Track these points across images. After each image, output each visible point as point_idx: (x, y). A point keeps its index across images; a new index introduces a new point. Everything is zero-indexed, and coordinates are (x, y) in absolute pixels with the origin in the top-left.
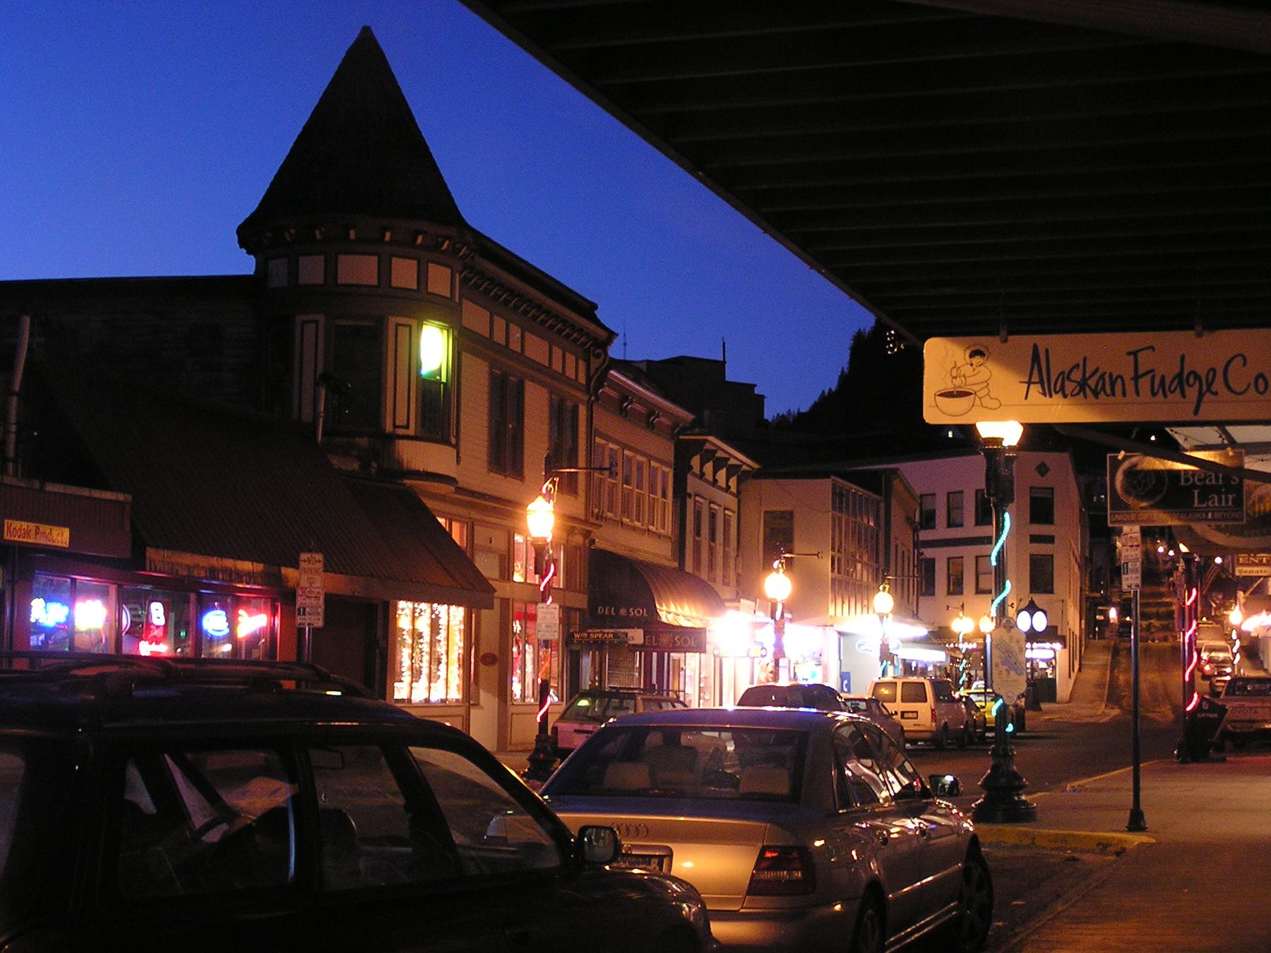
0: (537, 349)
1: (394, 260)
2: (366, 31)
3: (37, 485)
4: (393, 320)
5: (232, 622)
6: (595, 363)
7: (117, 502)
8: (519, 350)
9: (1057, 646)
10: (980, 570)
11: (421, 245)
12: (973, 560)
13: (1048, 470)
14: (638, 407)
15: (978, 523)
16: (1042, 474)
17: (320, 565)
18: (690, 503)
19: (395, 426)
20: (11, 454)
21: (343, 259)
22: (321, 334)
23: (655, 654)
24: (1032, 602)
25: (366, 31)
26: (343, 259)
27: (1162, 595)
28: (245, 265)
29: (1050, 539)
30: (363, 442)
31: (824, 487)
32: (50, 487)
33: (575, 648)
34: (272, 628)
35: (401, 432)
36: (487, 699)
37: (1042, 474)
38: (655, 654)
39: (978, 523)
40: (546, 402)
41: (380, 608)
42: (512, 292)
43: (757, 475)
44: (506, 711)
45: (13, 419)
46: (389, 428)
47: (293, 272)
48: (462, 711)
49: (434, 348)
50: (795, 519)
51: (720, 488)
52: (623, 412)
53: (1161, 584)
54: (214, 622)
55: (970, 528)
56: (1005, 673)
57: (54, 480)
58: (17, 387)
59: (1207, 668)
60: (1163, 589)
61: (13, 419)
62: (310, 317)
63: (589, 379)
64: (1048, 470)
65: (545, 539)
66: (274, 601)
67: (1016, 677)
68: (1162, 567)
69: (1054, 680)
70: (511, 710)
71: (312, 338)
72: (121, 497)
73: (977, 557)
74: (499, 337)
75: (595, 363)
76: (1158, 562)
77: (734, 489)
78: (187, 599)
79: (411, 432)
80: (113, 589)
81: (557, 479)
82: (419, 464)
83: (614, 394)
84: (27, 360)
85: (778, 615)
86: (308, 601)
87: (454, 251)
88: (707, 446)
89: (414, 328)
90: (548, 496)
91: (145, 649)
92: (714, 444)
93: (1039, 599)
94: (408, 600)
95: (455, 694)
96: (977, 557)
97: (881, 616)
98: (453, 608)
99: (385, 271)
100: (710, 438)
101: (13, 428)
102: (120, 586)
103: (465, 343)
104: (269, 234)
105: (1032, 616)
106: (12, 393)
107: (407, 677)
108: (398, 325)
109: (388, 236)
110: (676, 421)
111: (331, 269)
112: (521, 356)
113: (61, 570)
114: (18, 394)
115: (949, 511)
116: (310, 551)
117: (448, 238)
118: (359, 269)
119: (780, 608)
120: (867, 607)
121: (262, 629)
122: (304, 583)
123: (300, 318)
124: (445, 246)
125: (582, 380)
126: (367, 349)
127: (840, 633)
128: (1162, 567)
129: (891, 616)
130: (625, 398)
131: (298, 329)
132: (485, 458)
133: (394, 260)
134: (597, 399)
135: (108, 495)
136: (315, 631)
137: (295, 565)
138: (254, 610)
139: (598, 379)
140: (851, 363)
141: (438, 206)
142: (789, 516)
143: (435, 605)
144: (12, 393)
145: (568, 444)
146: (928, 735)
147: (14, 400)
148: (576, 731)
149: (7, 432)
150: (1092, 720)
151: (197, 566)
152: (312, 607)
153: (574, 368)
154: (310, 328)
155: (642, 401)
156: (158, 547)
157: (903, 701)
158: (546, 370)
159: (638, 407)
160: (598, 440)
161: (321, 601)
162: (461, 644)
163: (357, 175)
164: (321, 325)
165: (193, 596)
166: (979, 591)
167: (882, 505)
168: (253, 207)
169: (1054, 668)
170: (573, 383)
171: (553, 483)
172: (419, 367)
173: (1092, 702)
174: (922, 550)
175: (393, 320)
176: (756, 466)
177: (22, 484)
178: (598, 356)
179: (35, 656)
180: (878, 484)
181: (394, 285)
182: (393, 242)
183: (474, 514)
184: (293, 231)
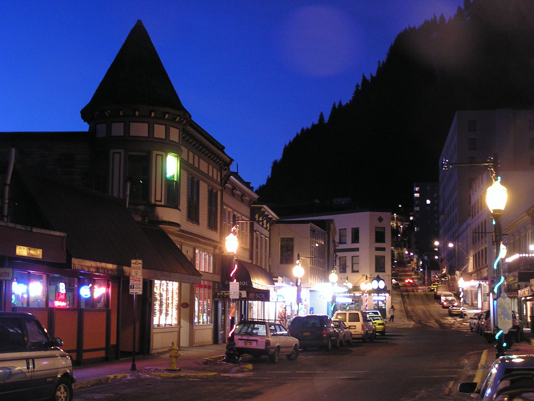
0: (204, 166)
1: (155, 125)
2: (139, 22)
3: (29, 229)
4: (155, 153)
5: (92, 289)
6: (225, 173)
7: (60, 236)
8: (197, 167)
9: (387, 295)
10: (354, 263)
11: (167, 119)
12: (351, 258)
13: (382, 220)
14: (238, 192)
15: (353, 242)
16: (380, 222)
17: (141, 266)
18: (255, 233)
19: (156, 201)
20: (6, 214)
21: (132, 125)
22: (122, 159)
23: (243, 301)
24: (378, 276)
25: (139, 22)
26: (132, 125)
27: (407, 271)
28: (85, 127)
29: (383, 249)
30: (141, 208)
31: (307, 227)
32: (34, 230)
33: (216, 299)
34: (107, 293)
35: (158, 203)
36: (185, 324)
37: (380, 222)
38: (243, 301)
39: (353, 242)
40: (207, 190)
41: (148, 283)
42: (197, 141)
43: (278, 222)
44: (193, 329)
45: (7, 196)
46: (153, 201)
47: (109, 129)
48: (177, 329)
49: (172, 166)
50: (295, 241)
51: (264, 228)
52: (233, 195)
53: (406, 267)
54: (85, 292)
55: (349, 245)
56: (503, 319)
57: (36, 226)
58: (8, 182)
59: (445, 303)
60: (406, 269)
61: (7, 196)
62: (117, 151)
63: (221, 180)
64: (382, 220)
65: (233, 253)
66: (108, 281)
67: (508, 321)
68: (406, 260)
69: (385, 309)
70: (195, 328)
71: (118, 159)
72: (62, 234)
73: (352, 257)
74: (191, 162)
75: (225, 173)
76: (403, 258)
77: (268, 229)
78: (76, 279)
79: (163, 203)
80: (45, 276)
81: (238, 225)
82: (166, 218)
83: (230, 186)
84: (13, 168)
85: (299, 284)
86: (135, 282)
87: (180, 122)
88: (263, 210)
89: (164, 156)
90: (234, 233)
91: (57, 304)
92: (265, 209)
93: (381, 275)
94: (158, 279)
95: (175, 322)
96: (352, 257)
97: (333, 284)
98: (174, 282)
99: (151, 130)
100: (264, 206)
101: (7, 201)
102: (48, 275)
103: (184, 165)
104: (97, 113)
105: (378, 282)
106: (6, 185)
107: (158, 313)
108: (157, 155)
109: (153, 114)
110: (252, 198)
111: (127, 129)
112: (198, 170)
113: (26, 268)
114: (9, 185)
115: (340, 237)
116: (136, 259)
117: (178, 115)
118: (139, 129)
119: (299, 281)
120: (326, 280)
121: (104, 294)
122: (133, 273)
123: (112, 151)
124: (177, 120)
125: (219, 180)
126: (143, 166)
127: (311, 291)
128: (406, 260)
129: (336, 284)
130: (234, 188)
131: (154, 159)
132: (186, 215)
133: (155, 125)
134: (225, 189)
135: (57, 233)
136: (138, 296)
137: (129, 265)
138: (100, 286)
139: (225, 180)
140: (272, 173)
141: (173, 101)
142: (292, 240)
143: (168, 282)
144: (6, 185)
145: (214, 209)
146: (360, 336)
147: (7, 189)
148: (239, 339)
149: (3, 203)
150: (405, 327)
151: (91, 267)
152: (137, 285)
153: (216, 175)
154: (117, 156)
155: (241, 190)
156: (76, 258)
157: (349, 321)
158: (207, 176)
159: (238, 192)
160: (225, 207)
161: (141, 282)
162: (177, 299)
163: (136, 87)
164: (123, 154)
165: (76, 279)
166: (353, 271)
167: (327, 235)
168: (88, 102)
169: (385, 304)
170: (215, 181)
171: (236, 227)
172: (166, 173)
173: (401, 318)
174: (338, 254)
175: (155, 153)
176: (278, 218)
177: (23, 229)
178: (225, 170)
179: (14, 308)
180: (325, 225)
181: (155, 136)
182: (155, 117)
183: (182, 241)
184: (109, 112)
